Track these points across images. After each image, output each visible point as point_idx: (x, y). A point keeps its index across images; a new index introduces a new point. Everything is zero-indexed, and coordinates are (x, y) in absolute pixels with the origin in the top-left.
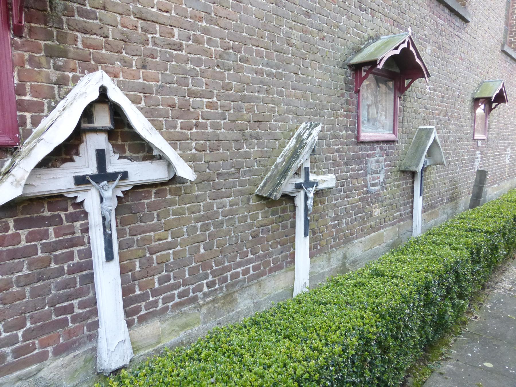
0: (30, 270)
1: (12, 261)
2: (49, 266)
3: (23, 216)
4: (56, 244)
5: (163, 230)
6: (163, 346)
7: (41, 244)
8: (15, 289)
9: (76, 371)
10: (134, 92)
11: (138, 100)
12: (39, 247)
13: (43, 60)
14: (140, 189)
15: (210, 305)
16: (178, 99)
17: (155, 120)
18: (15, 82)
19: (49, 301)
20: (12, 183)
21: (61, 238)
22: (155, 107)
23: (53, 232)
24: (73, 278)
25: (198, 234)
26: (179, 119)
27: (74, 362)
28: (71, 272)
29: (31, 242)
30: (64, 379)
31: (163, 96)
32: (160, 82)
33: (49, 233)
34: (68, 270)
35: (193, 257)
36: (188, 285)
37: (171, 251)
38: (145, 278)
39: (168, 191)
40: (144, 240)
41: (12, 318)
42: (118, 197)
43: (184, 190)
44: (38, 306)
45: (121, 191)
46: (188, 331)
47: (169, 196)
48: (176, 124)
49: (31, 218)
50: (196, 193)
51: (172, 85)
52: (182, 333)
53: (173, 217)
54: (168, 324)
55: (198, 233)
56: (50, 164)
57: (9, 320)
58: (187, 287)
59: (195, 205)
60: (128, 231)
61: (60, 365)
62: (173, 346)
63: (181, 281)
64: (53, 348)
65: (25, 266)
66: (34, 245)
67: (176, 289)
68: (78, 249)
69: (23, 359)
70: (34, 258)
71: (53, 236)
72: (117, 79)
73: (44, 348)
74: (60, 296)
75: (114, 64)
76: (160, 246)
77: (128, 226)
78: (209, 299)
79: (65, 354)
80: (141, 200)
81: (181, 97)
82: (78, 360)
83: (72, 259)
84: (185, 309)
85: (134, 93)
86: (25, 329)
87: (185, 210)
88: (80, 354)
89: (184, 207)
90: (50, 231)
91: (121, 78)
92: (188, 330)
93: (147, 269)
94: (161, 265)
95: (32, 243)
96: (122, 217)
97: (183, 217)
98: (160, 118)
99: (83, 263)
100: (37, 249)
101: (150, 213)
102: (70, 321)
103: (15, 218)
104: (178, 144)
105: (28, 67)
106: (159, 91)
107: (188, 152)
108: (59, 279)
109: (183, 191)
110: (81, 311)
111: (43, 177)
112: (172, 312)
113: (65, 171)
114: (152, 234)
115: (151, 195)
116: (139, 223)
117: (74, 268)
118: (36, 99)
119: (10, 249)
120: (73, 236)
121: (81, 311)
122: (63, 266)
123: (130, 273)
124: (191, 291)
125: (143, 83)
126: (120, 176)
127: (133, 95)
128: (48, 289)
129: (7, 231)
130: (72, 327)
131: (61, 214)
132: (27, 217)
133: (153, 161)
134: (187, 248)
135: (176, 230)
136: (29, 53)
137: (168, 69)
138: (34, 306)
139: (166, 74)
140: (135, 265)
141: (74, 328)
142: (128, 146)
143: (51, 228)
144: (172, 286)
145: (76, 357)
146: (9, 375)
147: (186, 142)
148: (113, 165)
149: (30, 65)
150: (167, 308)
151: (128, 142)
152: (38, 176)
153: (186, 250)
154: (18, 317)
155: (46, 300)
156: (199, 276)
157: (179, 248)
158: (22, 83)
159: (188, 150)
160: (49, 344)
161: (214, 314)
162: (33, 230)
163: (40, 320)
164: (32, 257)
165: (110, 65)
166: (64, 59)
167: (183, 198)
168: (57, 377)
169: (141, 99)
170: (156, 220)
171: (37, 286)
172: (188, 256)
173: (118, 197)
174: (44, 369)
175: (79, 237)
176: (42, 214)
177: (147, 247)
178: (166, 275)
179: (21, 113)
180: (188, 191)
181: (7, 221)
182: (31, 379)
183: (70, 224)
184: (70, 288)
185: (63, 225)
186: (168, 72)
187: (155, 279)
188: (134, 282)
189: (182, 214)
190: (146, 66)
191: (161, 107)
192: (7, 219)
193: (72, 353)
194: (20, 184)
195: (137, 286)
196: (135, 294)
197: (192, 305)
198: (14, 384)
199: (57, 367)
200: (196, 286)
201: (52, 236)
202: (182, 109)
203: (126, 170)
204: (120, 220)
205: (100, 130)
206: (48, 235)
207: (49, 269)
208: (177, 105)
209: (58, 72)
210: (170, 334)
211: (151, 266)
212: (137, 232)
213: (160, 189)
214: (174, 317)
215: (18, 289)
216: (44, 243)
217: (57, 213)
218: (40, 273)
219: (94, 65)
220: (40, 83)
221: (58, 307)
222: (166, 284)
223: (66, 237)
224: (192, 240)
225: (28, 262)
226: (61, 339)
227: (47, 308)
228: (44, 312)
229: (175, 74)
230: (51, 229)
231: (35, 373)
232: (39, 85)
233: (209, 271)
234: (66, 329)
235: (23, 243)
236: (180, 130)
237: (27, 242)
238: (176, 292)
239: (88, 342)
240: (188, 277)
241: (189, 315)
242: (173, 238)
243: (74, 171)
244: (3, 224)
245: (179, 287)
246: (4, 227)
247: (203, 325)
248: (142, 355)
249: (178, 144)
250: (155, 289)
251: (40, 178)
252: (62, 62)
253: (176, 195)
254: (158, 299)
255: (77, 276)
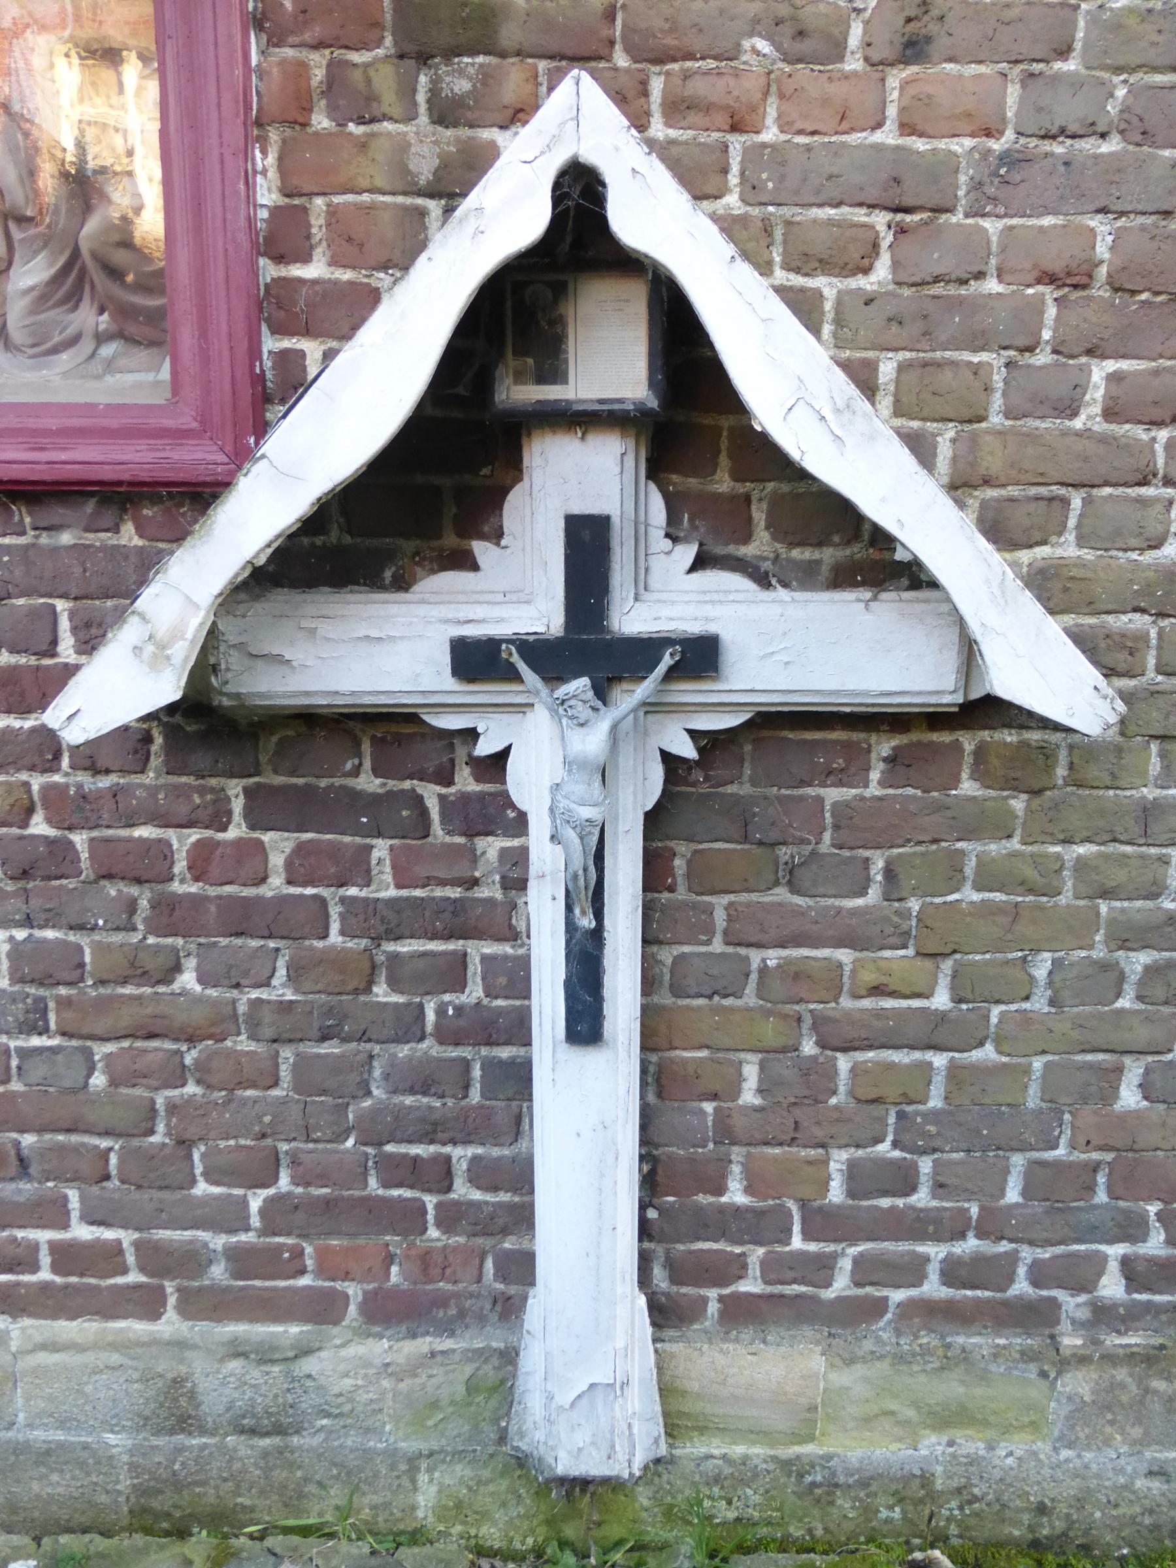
0: (297, 991)
1: (239, 941)
2: (368, 990)
3: (279, 780)
4: (398, 912)
5: (910, 952)
6: (822, 1457)
7: (343, 900)
8: (243, 1043)
9: (434, 1405)
10: (838, 205)
11: (854, 253)
12: (335, 911)
13: (385, 81)
14: (806, 729)
15: (1121, 1374)
16: (1118, 235)
17: (939, 365)
18: (261, 200)
19: (359, 1118)
20: (137, 650)
21: (418, 893)
22: (952, 290)
23: (388, 862)
24: (454, 1060)
25: (1121, 1012)
26: (1104, 357)
27: (430, 1372)
28: (447, 1035)
29: (304, 885)
30: (390, 1416)
31: (1015, 221)
32: (1010, 134)
33: (374, 862)
34: (437, 1025)
35: (1067, 1117)
36: (1011, 1241)
37: (940, 1060)
38: (781, 1144)
39: (968, 760)
40: (797, 976)
41: (232, 1142)
42: (667, 758)
43: (1071, 766)
44: (318, 1128)
45: (690, 731)
46: (971, 1444)
47: (968, 787)
48: (1080, 388)
49: (309, 790)
50: (1149, 793)
51: (1087, 145)
52: (933, 1439)
53: (976, 897)
54: (866, 1380)
55: (1124, 1003)
56: (388, 574)
57: (222, 1144)
58: (1004, 1247)
59: (1126, 856)
60: (720, 918)
61: (378, 1362)
62: (872, 1478)
63: (974, 1211)
64: (365, 1293)
65: (281, 972)
66: (315, 897)
67: (937, 1239)
68: (487, 951)
69: (260, 1289)
70: (312, 949)
71: (388, 877)
72: (743, 138)
73: (333, 1280)
74: (400, 1114)
75: (732, 55)
76: (875, 1023)
77: (726, 899)
78: (1125, 1341)
79: (404, 1329)
80: (803, 783)
81: (1141, 220)
82: (447, 1373)
83: (460, 985)
84: (978, 1342)
85: (832, 212)
86: (271, 1191)
87: (1058, 871)
88: (454, 1351)
89: (1058, 857)
90: (376, 854)
91: (770, 134)
92: (969, 1438)
93: (797, 1112)
94: (876, 1109)
95: (310, 891)
96: (696, 852)
97: (1041, 908)
98: (975, 350)
99: (500, 1011)
100: (327, 916)
101: (846, 853)
102: (430, 1217)
103: (252, 780)
104: (1076, 502)
105: (321, 121)
106: (991, 191)
107: (1134, 556)
108: (403, 1051)
109: (1061, 772)
110: (477, 1195)
111: (325, 628)
112: (898, 1333)
113: (422, 610)
114: (844, 956)
115: (868, 769)
116: (781, 894)
117: (462, 1022)
118: (347, 275)
119: (230, 897)
120: (469, 894)
121: (477, 1195)
122: (421, 1007)
123: (709, 1107)
124: (1022, 1271)
125: (897, 148)
126: (667, 661)
127: (830, 222)
128: (354, 1078)
129: (224, 829)
130: (439, 1244)
131: (425, 795)
132: (295, 786)
133: (884, 596)
134: (1038, 1064)
135: (987, 963)
136: (327, 52)
137: (1078, 45)
138: (300, 1122)
139: (1057, 78)
140: (740, 1078)
141: (445, 1247)
142: (765, 506)
143: (379, 842)
144: (918, 1219)
145: (439, 1359)
146: (214, 1325)
147: (1127, 499)
148: (655, 596)
149: (333, 111)
150: (880, 1306)
151: (770, 486)
152: (304, 624)
153: (1027, 1071)
154: (249, 1142)
155: (351, 1116)
156: (1084, 1216)
157: (987, 1053)
158: (296, 201)
159: (1133, 542)
160: (347, 1273)
161: (1139, 1421)
162: (310, 841)
163: (322, 1178)
164: (307, 943)
165: (711, 64)
166: (480, 59)
167: (1056, 806)
168: (363, 1397)
169: (876, 246)
170: (873, 895)
171: (318, 1056)
172: (1033, 1098)
173: (667, 758)
174: (323, 1354)
175: (490, 901)
176: (351, 782)
177: (811, 1011)
178: (892, 1162)
179: (287, 343)
180: (1094, 772)
181: (223, 790)
182: (276, 1369)
183: (460, 840)
184: (443, 1097)
185: (430, 839)
186: (1071, 65)
187: (833, 1166)
188: (723, 1148)
189: (1031, 891)
190: (928, 39)
191: (992, 285)
192: (223, 780)
193: (428, 1333)
194: (168, 658)
195: (736, 1169)
196: (724, 1199)
197: (1016, 1335)
198: (221, 1360)
199: (365, 1363)
200: (1055, 1258)
201: (384, 877)
202: (1133, 292)
203: (712, 628)
204: (689, 863)
205: (585, 413)
206: (368, 871)
207: (366, 1004)
208: (1103, 270)
209: (449, 133)
210: (867, 1421)
211: (817, 1101)
212: (762, 930)
213: (919, 744)
214: (900, 1359)
215: (251, 1046)
216: (354, 899)
217: (407, 784)
218: (329, 1012)
219: (627, 71)
220: (366, 197)
221: (391, 1156)
222: (885, 1202)
223: (439, 892)
224: (1075, 1034)
225: (291, 959)
226: (394, 1269)
227: (350, 1143)
228: (337, 1157)
229: (1118, 70)
230: (381, 849)
231: (291, 1354)
232: (359, 207)
233: (1153, 1209)
234: (414, 1244)
235: (276, 884)
236: (1100, 426)
237: (289, 882)
238: (936, 1252)
239: (494, 1317)
240: (1017, 1205)
241: (984, 1377)
242: (958, 1000)
243: (462, 615)
244: (209, 797)
245: (962, 1236)
246: (210, 810)
247: (1056, 1450)
248: (712, 1457)
249: (1076, 502)
250: (821, 1209)
251: (312, 632)
252: (470, 79)
253: (1016, 786)
254: (834, 1256)
255: (476, 1056)
